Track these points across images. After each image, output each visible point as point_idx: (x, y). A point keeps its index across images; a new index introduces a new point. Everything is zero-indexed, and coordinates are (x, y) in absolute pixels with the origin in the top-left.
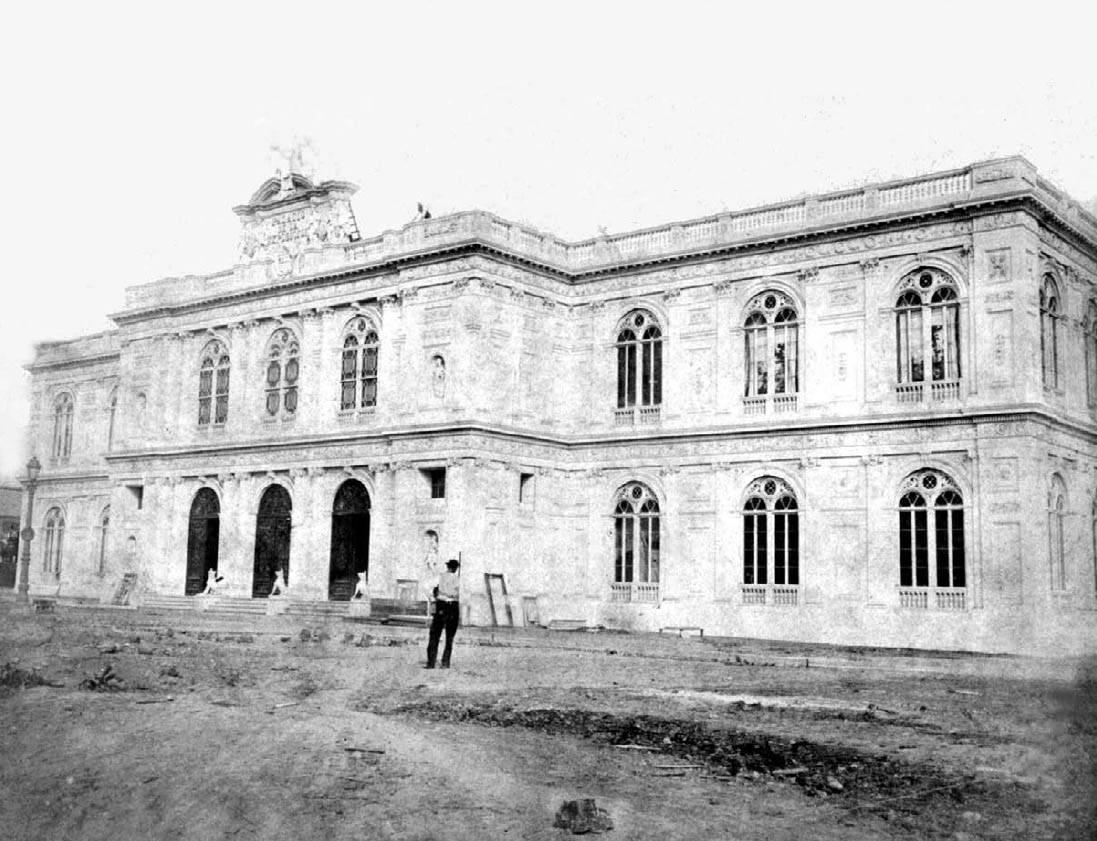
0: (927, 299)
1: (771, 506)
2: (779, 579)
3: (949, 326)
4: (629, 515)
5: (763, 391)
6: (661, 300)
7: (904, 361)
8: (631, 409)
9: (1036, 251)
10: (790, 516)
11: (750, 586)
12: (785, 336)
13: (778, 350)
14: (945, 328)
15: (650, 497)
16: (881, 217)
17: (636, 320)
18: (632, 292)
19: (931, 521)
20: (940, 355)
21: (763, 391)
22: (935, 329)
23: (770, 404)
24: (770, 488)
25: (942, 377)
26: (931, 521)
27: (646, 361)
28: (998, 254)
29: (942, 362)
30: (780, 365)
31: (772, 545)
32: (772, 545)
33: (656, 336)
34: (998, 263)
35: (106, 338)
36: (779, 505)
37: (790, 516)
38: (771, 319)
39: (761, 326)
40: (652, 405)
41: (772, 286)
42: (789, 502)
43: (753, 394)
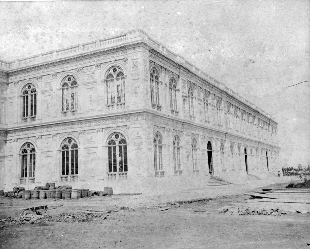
0: (70, 85)
1: (117, 143)
2: (72, 173)
3: (122, 85)
4: (114, 145)
5: (67, 109)
6: (123, 62)
7: (109, 97)
8: (27, 117)
9: (148, 60)
10: (67, 151)
11: (110, 173)
12: (119, 82)
13: (72, 95)
14: (121, 85)
15: (74, 142)
16: (15, 70)
17: (114, 71)
18: (67, 69)
19: (117, 149)
20: (119, 94)
21: (67, 109)
22: (118, 86)
23: (28, 119)
24: (117, 136)
25: (120, 101)
26: (117, 149)
27: (32, 101)
28: (135, 60)
29: (120, 97)
30: (72, 100)
31: (70, 163)
32: (70, 163)
33: (75, 85)
34: (135, 64)
35: (55, 53)
36: (120, 143)
37: (67, 151)
38: (70, 85)
39: (122, 77)
40: (34, 116)
41: (69, 74)
42: (124, 141)
43: (65, 110)
